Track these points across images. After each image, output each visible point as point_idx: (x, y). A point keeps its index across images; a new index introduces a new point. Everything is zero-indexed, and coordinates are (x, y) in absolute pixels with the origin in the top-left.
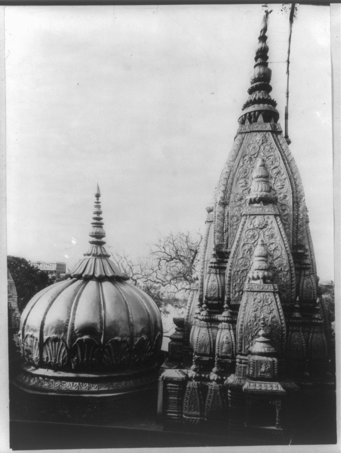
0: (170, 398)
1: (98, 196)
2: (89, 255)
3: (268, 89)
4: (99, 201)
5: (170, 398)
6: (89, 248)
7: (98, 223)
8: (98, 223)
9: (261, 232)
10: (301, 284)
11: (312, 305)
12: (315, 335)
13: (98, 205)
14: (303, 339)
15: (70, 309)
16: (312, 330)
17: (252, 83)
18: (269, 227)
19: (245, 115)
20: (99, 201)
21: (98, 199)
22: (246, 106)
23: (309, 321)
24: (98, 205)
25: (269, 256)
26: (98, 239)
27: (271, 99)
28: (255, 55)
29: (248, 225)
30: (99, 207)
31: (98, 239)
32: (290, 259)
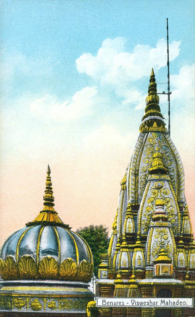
0: (189, 302)
1: (49, 173)
2: (44, 211)
3: (158, 108)
4: (50, 176)
5: (189, 302)
6: (43, 208)
7: (49, 189)
8: (49, 189)
9: (159, 191)
10: (183, 226)
11: (189, 237)
12: (192, 254)
13: (49, 179)
14: (124, 294)
15: (19, 241)
16: (190, 252)
17: (146, 111)
18: (163, 188)
19: (145, 122)
20: (50, 176)
21: (49, 175)
22: (145, 117)
23: (187, 247)
24: (49, 179)
25: (165, 205)
26: (49, 201)
27: (160, 113)
28: (148, 89)
29: (151, 186)
30: (50, 180)
31: (49, 201)
32: (177, 208)
